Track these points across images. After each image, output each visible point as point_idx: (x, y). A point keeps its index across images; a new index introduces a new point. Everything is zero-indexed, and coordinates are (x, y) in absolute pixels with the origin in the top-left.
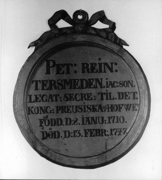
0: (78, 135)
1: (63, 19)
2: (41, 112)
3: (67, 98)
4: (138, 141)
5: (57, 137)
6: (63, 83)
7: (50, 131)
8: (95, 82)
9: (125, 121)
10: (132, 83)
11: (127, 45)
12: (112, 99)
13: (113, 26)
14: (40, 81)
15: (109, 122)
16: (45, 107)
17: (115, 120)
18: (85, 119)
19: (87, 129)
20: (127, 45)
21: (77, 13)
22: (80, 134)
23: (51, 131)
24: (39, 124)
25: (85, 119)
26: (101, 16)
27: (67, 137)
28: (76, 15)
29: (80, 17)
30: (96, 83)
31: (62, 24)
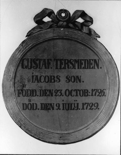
0: (60, 94)
1: (82, 18)
2: (77, 81)
3: (35, 63)
4: (92, 136)
5: (25, 109)
6: (73, 63)
7: (29, 103)
8: (49, 106)
9: (98, 107)
10: (80, 77)
11: (99, 37)
12: (91, 68)
13: (91, 21)
14: (28, 59)
15: (83, 109)
16: (76, 81)
17: (89, 107)
18: (35, 77)
19: (92, 59)
20: (99, 37)
21: (61, 11)
22: (61, 94)
23: (30, 102)
24: (91, 110)
25: (35, 77)
26: (83, 14)
27: (35, 110)
28: (66, 16)
29: (63, 15)
30: (50, 107)
31: (47, 19)
